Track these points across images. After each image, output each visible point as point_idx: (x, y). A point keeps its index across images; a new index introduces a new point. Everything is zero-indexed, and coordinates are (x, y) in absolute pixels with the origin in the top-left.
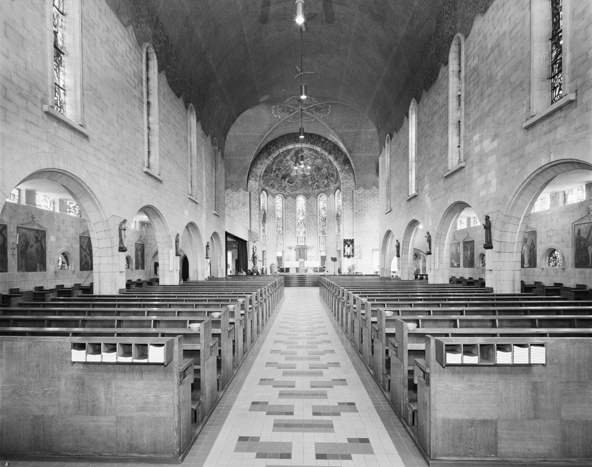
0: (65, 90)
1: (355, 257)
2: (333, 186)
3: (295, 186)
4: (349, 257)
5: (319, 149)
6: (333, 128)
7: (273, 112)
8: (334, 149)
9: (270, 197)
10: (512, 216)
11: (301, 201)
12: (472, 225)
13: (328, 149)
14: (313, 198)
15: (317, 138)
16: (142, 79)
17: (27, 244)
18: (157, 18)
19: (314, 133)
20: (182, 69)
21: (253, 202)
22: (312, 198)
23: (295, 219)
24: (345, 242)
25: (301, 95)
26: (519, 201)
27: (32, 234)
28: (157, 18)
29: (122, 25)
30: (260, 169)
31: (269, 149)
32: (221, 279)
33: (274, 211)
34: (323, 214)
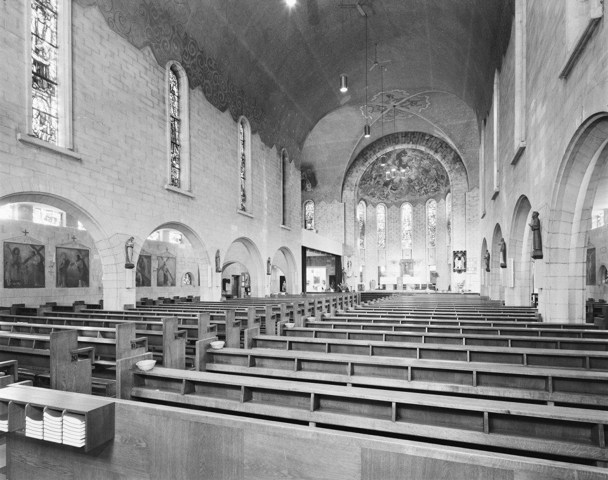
0: (57, 118)
1: (467, 272)
2: (443, 190)
3: (400, 193)
4: (460, 271)
5: (423, 149)
6: (436, 123)
7: (363, 114)
8: (442, 146)
9: (370, 206)
10: (561, 211)
11: (407, 209)
12: (599, 226)
13: (434, 147)
14: (421, 205)
15: (421, 136)
16: (164, 98)
17: (67, 262)
18: (186, 34)
19: (416, 130)
20: (228, 82)
21: (347, 213)
22: (420, 206)
23: (399, 229)
24: (455, 254)
25: (341, 88)
26: (567, 187)
27: (73, 253)
28: (186, 34)
29: (133, 48)
30: (356, 177)
31: (365, 155)
32: (296, 296)
33: (374, 222)
34: (433, 223)
